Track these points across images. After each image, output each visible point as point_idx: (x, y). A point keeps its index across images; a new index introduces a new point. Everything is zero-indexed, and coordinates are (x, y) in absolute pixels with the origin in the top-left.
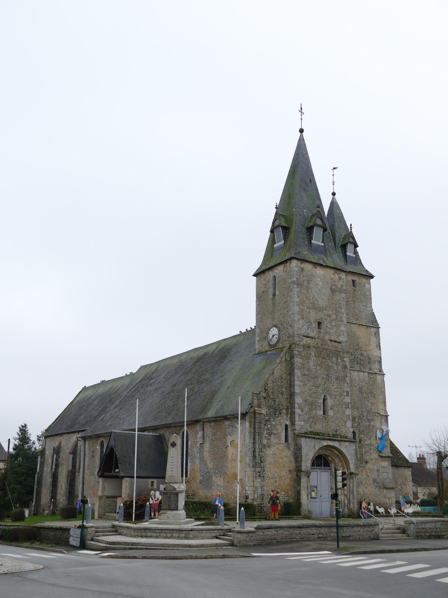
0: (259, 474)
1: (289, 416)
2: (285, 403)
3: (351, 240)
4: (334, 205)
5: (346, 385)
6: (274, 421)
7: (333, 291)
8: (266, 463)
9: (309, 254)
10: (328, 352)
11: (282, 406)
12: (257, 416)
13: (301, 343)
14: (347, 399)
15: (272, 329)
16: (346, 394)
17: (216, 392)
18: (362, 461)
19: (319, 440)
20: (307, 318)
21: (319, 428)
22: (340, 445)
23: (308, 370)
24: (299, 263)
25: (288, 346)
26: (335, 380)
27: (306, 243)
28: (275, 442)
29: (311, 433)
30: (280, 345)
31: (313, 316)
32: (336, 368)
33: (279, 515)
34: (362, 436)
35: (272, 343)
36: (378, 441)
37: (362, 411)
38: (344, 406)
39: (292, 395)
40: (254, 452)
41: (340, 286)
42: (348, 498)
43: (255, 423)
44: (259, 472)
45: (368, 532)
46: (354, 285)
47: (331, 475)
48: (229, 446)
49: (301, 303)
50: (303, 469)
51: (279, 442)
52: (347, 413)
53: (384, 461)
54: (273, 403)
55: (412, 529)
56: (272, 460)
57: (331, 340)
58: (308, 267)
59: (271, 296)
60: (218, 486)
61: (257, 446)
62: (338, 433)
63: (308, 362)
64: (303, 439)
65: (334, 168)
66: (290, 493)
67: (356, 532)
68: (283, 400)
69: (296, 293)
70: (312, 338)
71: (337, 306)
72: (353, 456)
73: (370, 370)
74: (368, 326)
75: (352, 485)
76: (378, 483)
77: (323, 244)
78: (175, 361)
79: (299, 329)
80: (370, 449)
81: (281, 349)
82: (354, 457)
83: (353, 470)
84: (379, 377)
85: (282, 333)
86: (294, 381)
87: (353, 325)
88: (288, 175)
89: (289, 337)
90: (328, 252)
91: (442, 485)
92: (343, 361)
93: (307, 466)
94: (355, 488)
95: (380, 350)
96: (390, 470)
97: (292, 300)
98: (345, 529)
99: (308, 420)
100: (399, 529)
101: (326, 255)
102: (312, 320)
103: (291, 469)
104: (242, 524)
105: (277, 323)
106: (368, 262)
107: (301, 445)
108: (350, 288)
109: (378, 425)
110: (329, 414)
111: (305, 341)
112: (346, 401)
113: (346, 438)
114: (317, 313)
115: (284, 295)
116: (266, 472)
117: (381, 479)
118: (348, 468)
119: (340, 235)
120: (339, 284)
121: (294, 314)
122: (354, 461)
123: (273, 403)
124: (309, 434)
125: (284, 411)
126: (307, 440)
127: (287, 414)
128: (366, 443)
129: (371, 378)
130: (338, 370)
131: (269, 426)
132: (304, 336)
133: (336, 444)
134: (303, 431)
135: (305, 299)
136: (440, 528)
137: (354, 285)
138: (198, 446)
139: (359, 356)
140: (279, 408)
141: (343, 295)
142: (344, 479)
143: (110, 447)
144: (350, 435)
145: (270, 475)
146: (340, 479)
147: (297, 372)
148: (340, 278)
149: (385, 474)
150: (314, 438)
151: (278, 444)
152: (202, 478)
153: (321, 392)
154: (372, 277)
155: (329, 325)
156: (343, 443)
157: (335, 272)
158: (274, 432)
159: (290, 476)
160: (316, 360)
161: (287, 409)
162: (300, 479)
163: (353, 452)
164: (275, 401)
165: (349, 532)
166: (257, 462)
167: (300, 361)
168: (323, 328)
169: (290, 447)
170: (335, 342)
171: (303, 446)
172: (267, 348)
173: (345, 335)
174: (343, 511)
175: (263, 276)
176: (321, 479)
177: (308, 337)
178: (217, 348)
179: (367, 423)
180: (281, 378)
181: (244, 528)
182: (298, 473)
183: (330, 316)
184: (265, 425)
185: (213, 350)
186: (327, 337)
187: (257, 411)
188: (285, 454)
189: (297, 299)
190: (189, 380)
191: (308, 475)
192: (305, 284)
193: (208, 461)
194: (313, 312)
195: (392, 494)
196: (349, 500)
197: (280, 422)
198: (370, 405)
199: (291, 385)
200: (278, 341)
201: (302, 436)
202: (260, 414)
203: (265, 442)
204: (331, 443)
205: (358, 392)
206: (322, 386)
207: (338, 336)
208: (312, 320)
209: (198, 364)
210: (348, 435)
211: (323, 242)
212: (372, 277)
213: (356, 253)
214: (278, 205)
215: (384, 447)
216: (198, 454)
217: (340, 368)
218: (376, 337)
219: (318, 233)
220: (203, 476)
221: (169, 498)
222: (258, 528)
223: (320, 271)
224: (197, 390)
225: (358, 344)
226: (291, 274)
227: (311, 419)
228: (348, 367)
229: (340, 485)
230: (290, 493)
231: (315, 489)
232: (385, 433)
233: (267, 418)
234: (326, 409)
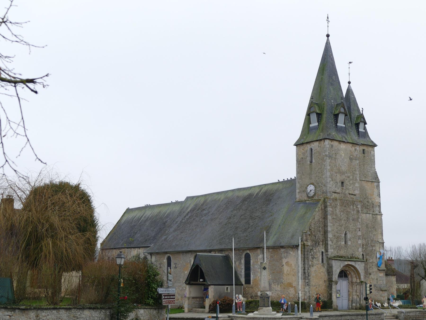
2: (321, 238)
3: (362, 120)
4: (349, 90)
5: (359, 224)
6: (315, 249)
7: (351, 159)
8: (311, 277)
9: (336, 134)
10: (347, 202)
12: (306, 247)
13: (332, 197)
14: (359, 233)
15: (310, 186)
17: (270, 227)
18: (367, 273)
21: (342, 253)
23: (336, 215)
25: (323, 199)
27: (334, 126)
30: (316, 198)
31: (339, 178)
33: (321, 308)
34: (368, 257)
35: (309, 196)
36: (378, 260)
38: (357, 238)
39: (326, 233)
41: (355, 156)
43: (304, 251)
46: (364, 153)
49: (332, 170)
50: (334, 280)
52: (359, 243)
53: (381, 273)
55: (402, 316)
57: (350, 194)
58: (335, 143)
59: (309, 163)
60: (276, 290)
64: (333, 261)
65: (350, 63)
66: (325, 295)
68: (320, 236)
69: (328, 163)
70: (338, 193)
71: (354, 170)
73: (373, 212)
74: (372, 182)
76: (377, 287)
77: (344, 126)
78: (222, 197)
79: (330, 187)
81: (318, 201)
82: (363, 271)
83: (362, 280)
84: (379, 217)
85: (318, 189)
86: (327, 223)
87: (363, 182)
88: (319, 70)
89: (323, 193)
90: (347, 131)
91: (414, 285)
96: (384, 278)
97: (326, 167)
98: (371, 316)
100: (394, 316)
101: (346, 133)
102: (338, 181)
103: (325, 280)
104: (311, 314)
105: (314, 182)
106: (373, 135)
107: (332, 265)
108: (362, 155)
109: (377, 249)
111: (334, 195)
112: (359, 234)
113: (358, 259)
115: (319, 163)
116: (311, 282)
118: (360, 278)
119: (354, 114)
120: (355, 154)
121: (327, 177)
125: (321, 243)
126: (336, 261)
134: (333, 256)
137: (364, 153)
138: (259, 264)
139: (367, 203)
141: (358, 162)
142: (371, 289)
143: (195, 264)
144: (361, 257)
146: (368, 289)
147: (329, 217)
148: (356, 150)
150: (340, 260)
154: (375, 146)
156: (357, 262)
157: (353, 146)
158: (315, 256)
159: (325, 284)
161: (323, 241)
162: (332, 286)
164: (315, 237)
166: (306, 276)
167: (331, 209)
170: (352, 194)
172: (306, 198)
173: (359, 189)
174: (356, 305)
175: (302, 147)
176: (342, 285)
177: (336, 193)
178: (260, 191)
179: (371, 248)
180: (319, 221)
181: (312, 316)
182: (330, 282)
183: (349, 177)
184: (310, 252)
185: (256, 192)
186: (347, 192)
189: (329, 167)
190: (242, 215)
191: (336, 283)
192: (334, 156)
194: (338, 175)
195: (385, 294)
196: (360, 299)
198: (373, 236)
200: (315, 195)
201: (333, 259)
202: (307, 246)
203: (310, 263)
204: (350, 263)
207: (354, 190)
208: (338, 181)
209: (246, 203)
211: (344, 124)
212: (375, 146)
213: (365, 128)
215: (381, 264)
217: (355, 212)
218: (377, 189)
219: (341, 118)
221: (264, 300)
222: (320, 316)
223: (343, 146)
224: (252, 224)
227: (337, 248)
228: (360, 211)
229: (368, 292)
230: (325, 295)
231: (339, 292)
232: (382, 254)
233: (311, 248)
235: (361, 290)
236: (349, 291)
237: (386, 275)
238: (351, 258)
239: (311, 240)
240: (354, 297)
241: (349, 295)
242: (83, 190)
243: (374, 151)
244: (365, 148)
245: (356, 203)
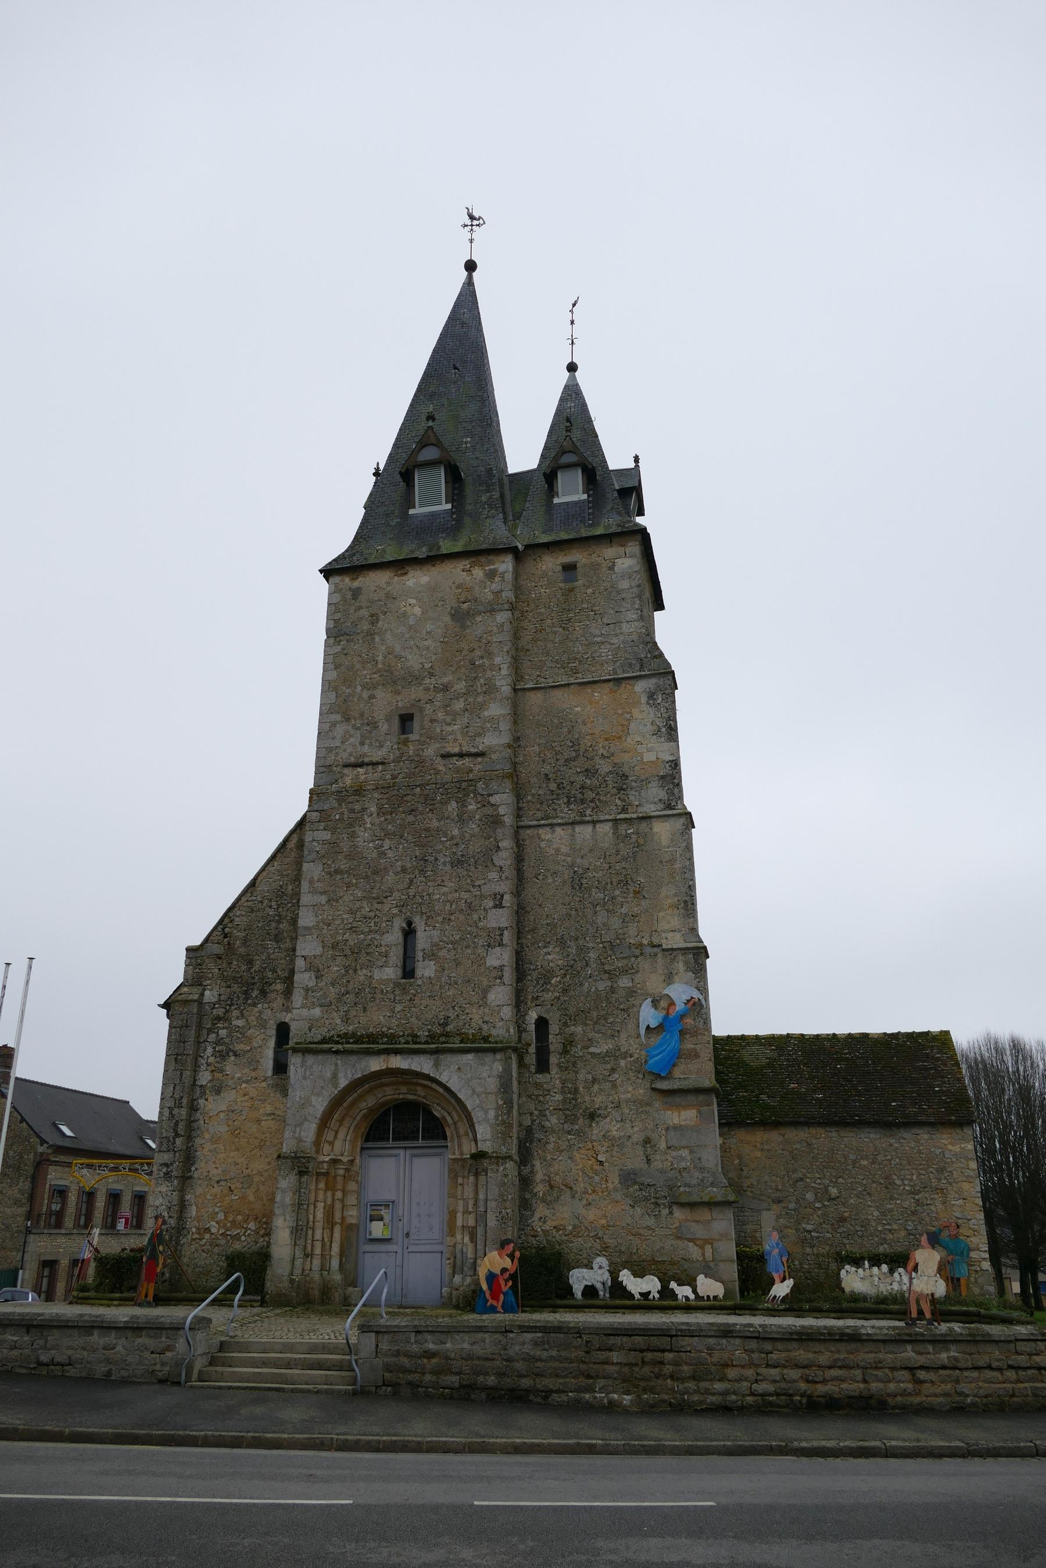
0: (165, 1170)
5: (493, 875)
11: (274, 971)
16: (491, 904)
19: (354, 1058)
20: (362, 715)
21: (378, 1018)
22: (437, 1065)
24: (347, 580)
26: (448, 867)
28: (238, 1075)
29: (345, 1037)
32: (456, 832)
37: (581, 949)
41: (490, 597)
44: (167, 1165)
45: (147, 1354)
51: (253, 1074)
53: (679, 1107)
54: (244, 968)
56: (224, 1129)
57: (446, 756)
62: (448, 1029)
67: (95, 1351)
72: (492, 1098)
73: (624, 810)
76: (643, 1186)
80: (613, 1070)
84: (662, 830)
87: (558, 693)
92: (485, 804)
93: (300, 1140)
94: (492, 1205)
96: (713, 1136)
99: (339, 1000)
114: (398, 693)
117: (662, 1171)
122: (492, 1114)
123: (244, 968)
124: (337, 1043)
126: (310, 1059)
128: (592, 1050)
129: (627, 836)
130: (462, 837)
131: (223, 1033)
132: (346, 766)
133: (422, 1064)
134: (317, 1035)
135: (358, 666)
136: (530, 1359)
139: (581, 778)
145: (214, 1172)
149: (685, 1153)
151: (247, 1082)
153: (395, 911)
155: (440, 715)
158: (239, 1047)
160: (381, 823)
163: (493, 1084)
164: (250, 963)
165: (69, 1348)
177: (361, 765)
179: (602, 986)
184: (210, 1031)
186: (431, 751)
188: (269, 1109)
197: (259, 1017)
204: (398, 1062)
205: (568, 889)
206: (396, 894)
210: (494, 1032)
214: (382, 467)
225: (576, 743)
227: (350, 998)
233: (220, 1012)
237: (728, 1123)
238: (432, 1037)
239: (224, 978)
244: (575, 556)
245: (480, 785)
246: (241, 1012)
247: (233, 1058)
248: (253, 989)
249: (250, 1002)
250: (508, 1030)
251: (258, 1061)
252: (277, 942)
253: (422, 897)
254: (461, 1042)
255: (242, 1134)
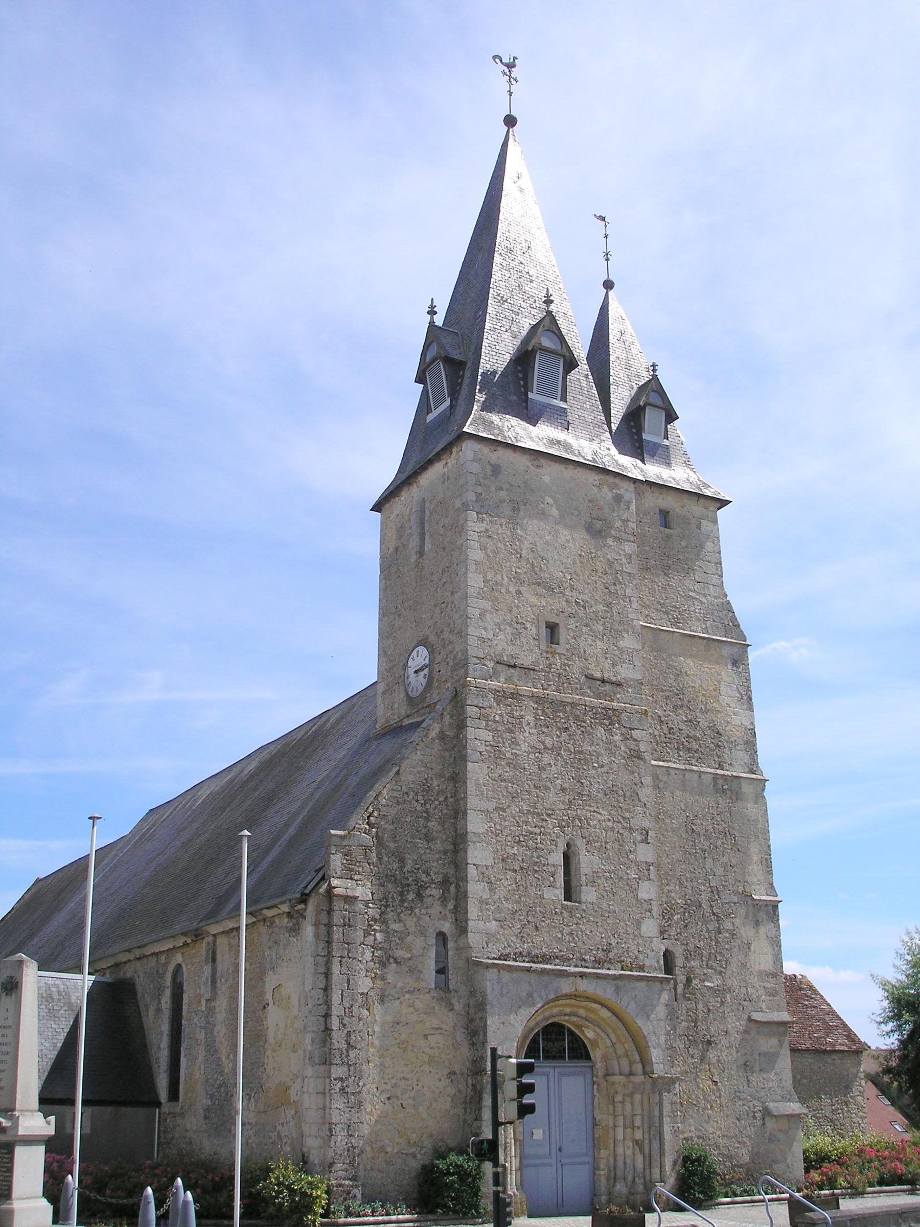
0: (339, 1085)
1: (450, 906)
2: (437, 868)
3: (655, 399)
12: (338, 905)
14: (645, 853)
15: (414, 653)
16: (639, 838)
28: (400, 985)
31: (535, 605)
39: (458, 843)
40: (327, 1016)
42: (647, 1151)
43: (329, 925)
44: (341, 1079)
47: (594, 1083)
48: (271, 1003)
54: (395, 866)
61: (336, 998)
63: (515, 743)
75: (657, 1113)
79: (482, 640)
95: (751, 709)
103: (457, 1068)
107: (484, 995)
110: (583, 898)
112: (641, 858)
125: (436, 892)
127: (444, 900)
140: (416, 880)
151: (409, 992)
152: (209, 1103)
158: (400, 953)
159: (451, 1091)
161: (445, 883)
164: (402, 860)
167: (487, 736)
168: (562, 641)
169: (454, 1001)
171: (490, 996)
180: (426, 787)
187: (336, 891)
188: (436, 1023)
193: (224, 1051)
198: (720, 871)
199: (458, 813)
212: (724, 503)
216: (203, 1031)
220: (212, 1097)
226: (462, 481)
234: (574, 883)
235: (650, 1117)
236: (595, 1124)
240: (620, 1150)
241: (595, 1144)
242: (11, 1212)
243: (715, 521)
246: (399, 915)
247: (394, 966)
248: (408, 891)
249: (405, 905)
250: (658, 962)
251: (421, 972)
252: (428, 842)
253: (580, 820)
254: (622, 969)
255: (409, 1048)
